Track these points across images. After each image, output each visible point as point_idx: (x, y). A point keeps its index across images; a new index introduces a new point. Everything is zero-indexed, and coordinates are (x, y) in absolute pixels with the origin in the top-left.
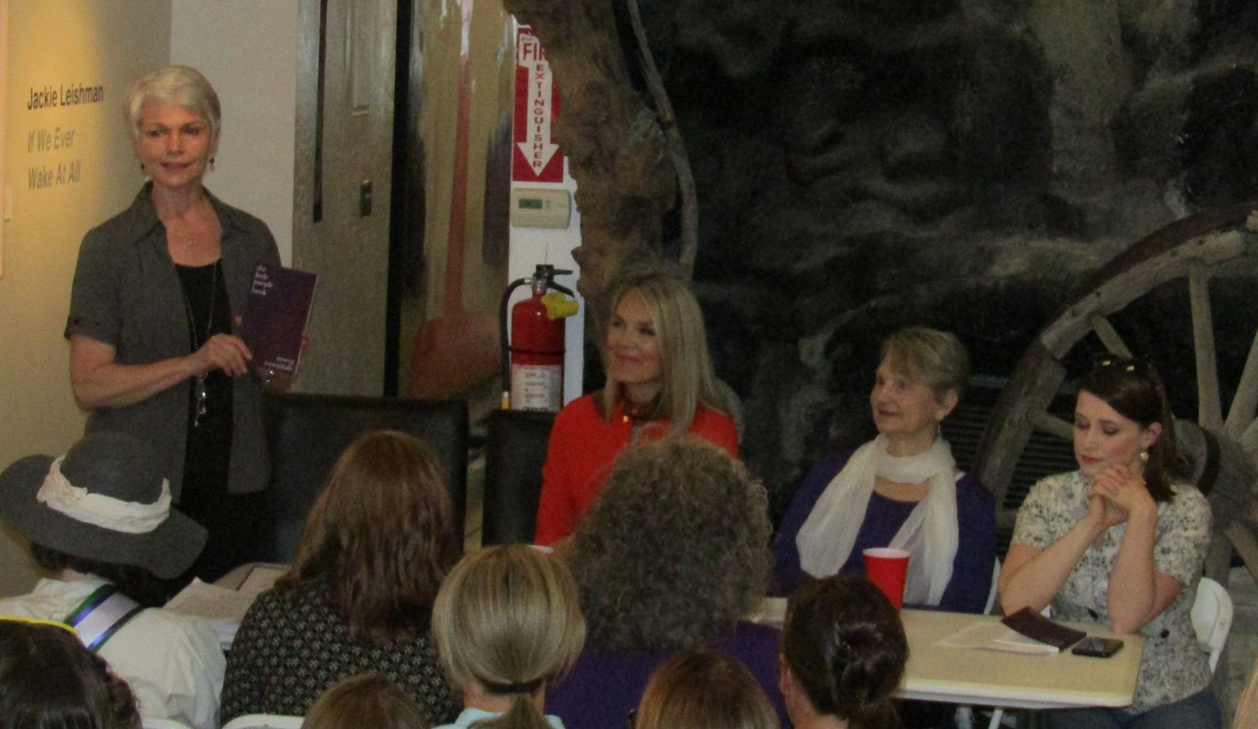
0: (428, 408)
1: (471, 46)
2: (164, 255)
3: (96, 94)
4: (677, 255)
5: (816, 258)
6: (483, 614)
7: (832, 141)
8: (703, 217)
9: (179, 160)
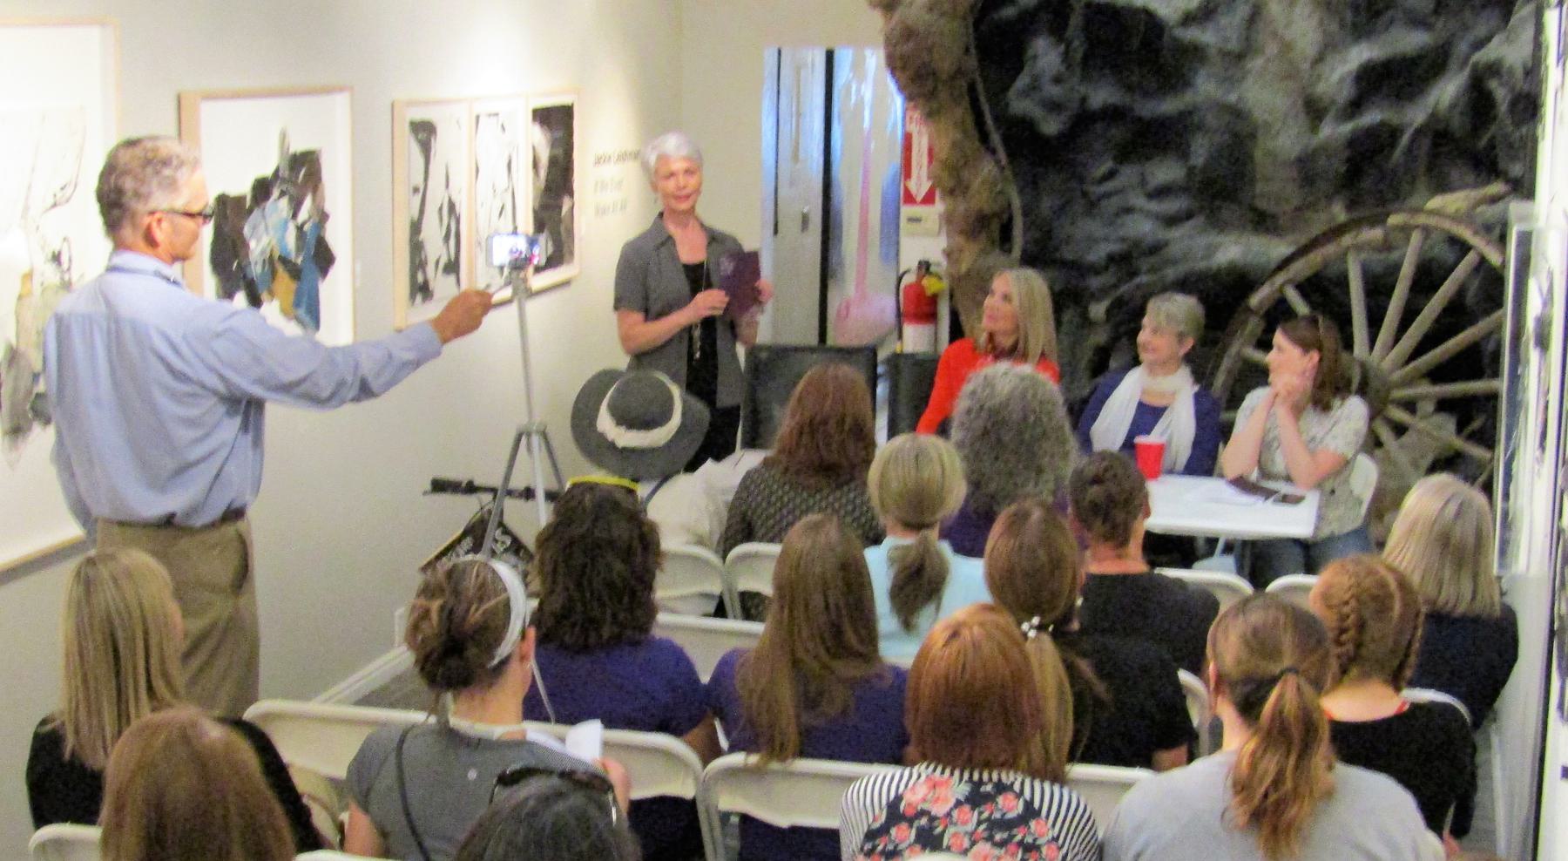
0: (846, 353)
1: (871, 119)
2: (674, 257)
3: (636, 155)
4: (1010, 251)
5: (1098, 254)
6: (118, 600)
7: (1111, 175)
8: (1027, 229)
9: (684, 192)
